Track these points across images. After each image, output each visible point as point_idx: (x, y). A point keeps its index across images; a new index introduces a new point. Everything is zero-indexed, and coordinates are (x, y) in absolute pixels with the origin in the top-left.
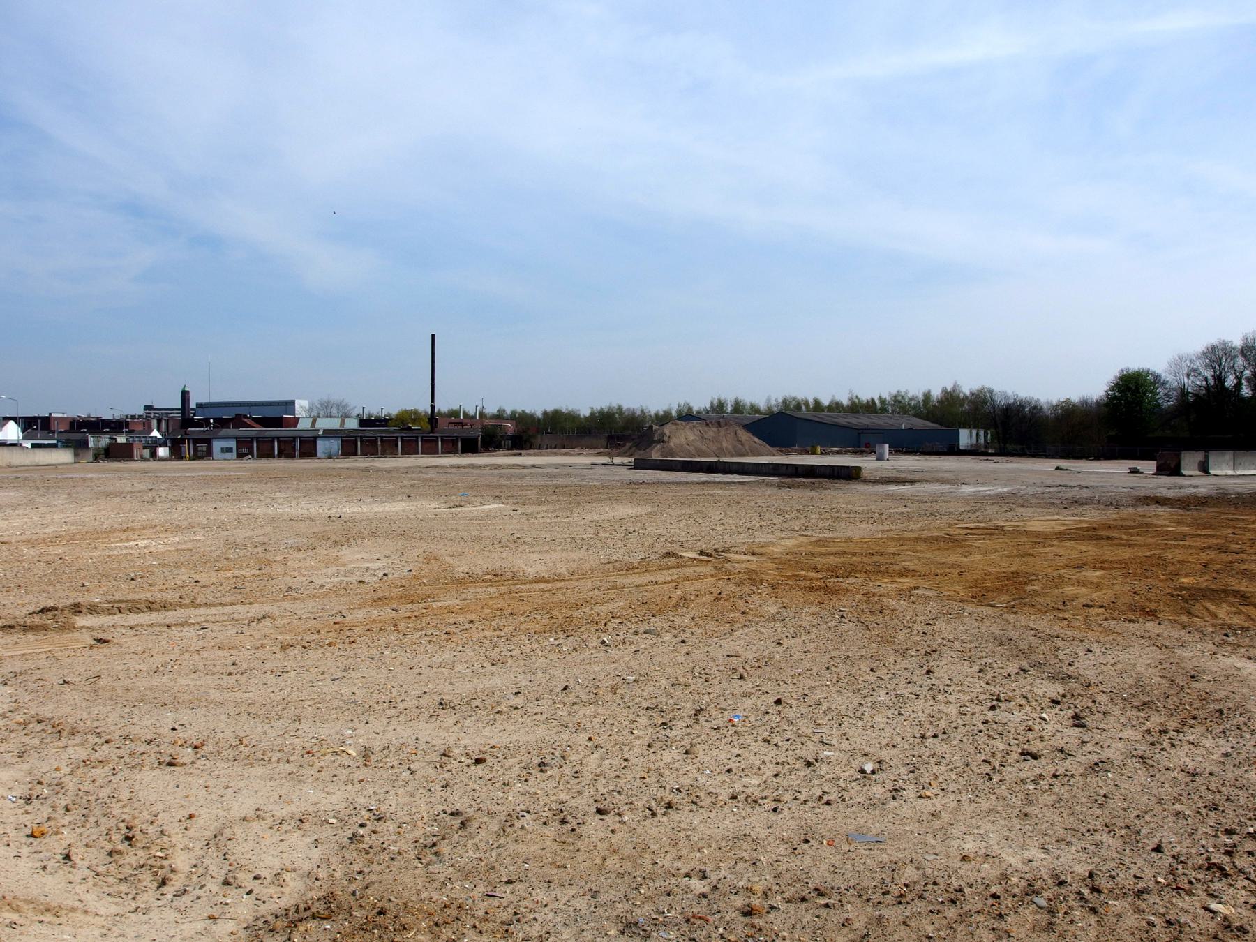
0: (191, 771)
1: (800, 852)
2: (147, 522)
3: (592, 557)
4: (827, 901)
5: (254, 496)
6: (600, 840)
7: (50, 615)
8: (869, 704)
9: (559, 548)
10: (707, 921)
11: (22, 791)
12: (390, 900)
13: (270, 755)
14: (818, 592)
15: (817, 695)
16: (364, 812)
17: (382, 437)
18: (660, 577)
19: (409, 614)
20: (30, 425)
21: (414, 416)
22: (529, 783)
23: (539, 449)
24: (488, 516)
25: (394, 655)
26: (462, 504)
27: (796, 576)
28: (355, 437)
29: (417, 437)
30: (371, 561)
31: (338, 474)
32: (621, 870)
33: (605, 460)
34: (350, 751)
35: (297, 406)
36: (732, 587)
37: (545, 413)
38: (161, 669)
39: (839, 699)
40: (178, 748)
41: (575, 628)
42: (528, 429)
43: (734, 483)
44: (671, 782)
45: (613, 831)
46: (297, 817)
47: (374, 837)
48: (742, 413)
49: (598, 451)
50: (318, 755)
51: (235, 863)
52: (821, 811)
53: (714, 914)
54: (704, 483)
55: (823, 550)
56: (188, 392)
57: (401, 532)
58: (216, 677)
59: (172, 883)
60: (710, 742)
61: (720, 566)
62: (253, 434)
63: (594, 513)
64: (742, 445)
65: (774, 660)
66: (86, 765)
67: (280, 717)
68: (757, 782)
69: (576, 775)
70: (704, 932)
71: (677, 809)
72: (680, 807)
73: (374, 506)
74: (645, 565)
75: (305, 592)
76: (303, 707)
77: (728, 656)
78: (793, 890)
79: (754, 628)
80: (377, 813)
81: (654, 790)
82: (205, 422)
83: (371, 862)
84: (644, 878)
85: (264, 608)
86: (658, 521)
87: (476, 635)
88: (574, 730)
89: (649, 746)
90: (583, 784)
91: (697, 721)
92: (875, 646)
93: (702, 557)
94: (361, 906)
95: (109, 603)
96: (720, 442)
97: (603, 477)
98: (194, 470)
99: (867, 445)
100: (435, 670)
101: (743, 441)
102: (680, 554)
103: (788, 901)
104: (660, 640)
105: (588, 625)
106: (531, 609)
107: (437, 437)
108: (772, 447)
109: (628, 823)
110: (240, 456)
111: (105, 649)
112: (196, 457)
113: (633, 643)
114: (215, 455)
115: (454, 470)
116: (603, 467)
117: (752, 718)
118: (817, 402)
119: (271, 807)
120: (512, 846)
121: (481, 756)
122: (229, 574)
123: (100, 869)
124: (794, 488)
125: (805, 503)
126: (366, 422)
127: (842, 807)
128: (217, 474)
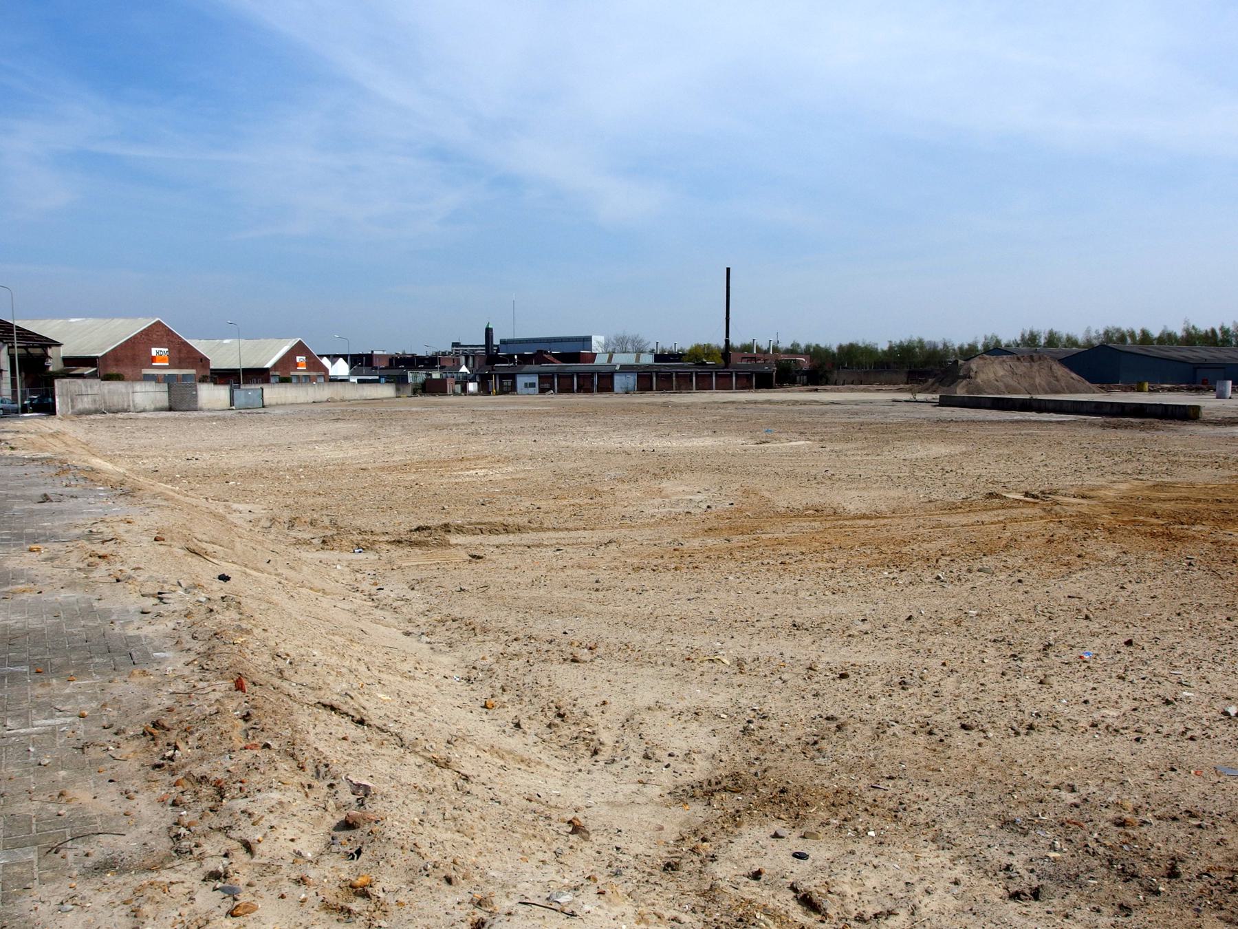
0: (592, 667)
1: (1167, 778)
2: (478, 453)
3: (913, 496)
4: (1199, 822)
5: (567, 429)
6: (968, 751)
7: (426, 533)
8: (1229, 652)
9: (874, 486)
10: (1081, 826)
11: (462, 673)
12: (788, 783)
13: (655, 659)
14: (1160, 539)
15: (1170, 639)
16: (748, 711)
17: (677, 372)
18: (986, 517)
19: (741, 544)
20: (360, 362)
21: (708, 351)
22: (893, 698)
23: (836, 384)
24: (797, 453)
25: (738, 581)
26: (769, 440)
27: (1134, 521)
28: (651, 372)
29: (712, 372)
30: (692, 493)
31: (639, 409)
32: (992, 778)
33: (907, 396)
34: (725, 660)
35: (594, 342)
36: (1064, 530)
37: (841, 348)
38: (536, 583)
39: (1194, 644)
40: (575, 648)
41: (907, 564)
42: (824, 364)
43: (1051, 422)
44: (1029, 707)
45: (980, 745)
46: (692, 710)
47: (762, 732)
48: (1057, 347)
49: (897, 387)
50: (697, 661)
51: (650, 742)
52: (1185, 744)
53: (1086, 822)
54: (1017, 421)
55: (1162, 495)
56: (492, 329)
57: (719, 467)
58: (585, 592)
59: (602, 753)
60: (1063, 675)
61: (1049, 508)
62: (554, 369)
63: (905, 452)
64: (1058, 380)
65: (1119, 604)
66: (505, 657)
67: (653, 629)
68: (1115, 714)
69: (936, 694)
70: (1079, 836)
71: (1039, 730)
72: (1042, 729)
73: (682, 441)
74: (965, 506)
75: (639, 521)
76: (671, 621)
77: (1069, 597)
78: (1163, 810)
79: (1094, 571)
80: (761, 713)
81: (1013, 713)
82: (509, 358)
83: (764, 752)
84: (1015, 786)
85: (606, 534)
86: (975, 461)
87: (811, 567)
88: (925, 656)
89: (1003, 674)
90: (944, 703)
91: (1046, 655)
92: (1231, 595)
93: (1027, 499)
94: (765, 785)
95: (471, 524)
96: (1033, 378)
97: (908, 415)
98: (504, 404)
99: (1205, 382)
100: (780, 595)
101: (1059, 377)
102: (1004, 495)
103: (1159, 818)
104: (995, 579)
105: (919, 562)
106: (858, 544)
107: (732, 372)
108: (1092, 383)
109: (992, 739)
110: (542, 391)
111: (480, 565)
112: (503, 391)
113: (968, 580)
114: (519, 391)
115: (752, 406)
116: (905, 403)
117: (1103, 656)
118: (1145, 334)
119: (668, 701)
120: (887, 750)
121: (844, 672)
122: (565, 502)
123: (545, 737)
124: (1121, 428)
125: (1136, 445)
126: (660, 357)
127: (1207, 743)
128: (526, 408)
